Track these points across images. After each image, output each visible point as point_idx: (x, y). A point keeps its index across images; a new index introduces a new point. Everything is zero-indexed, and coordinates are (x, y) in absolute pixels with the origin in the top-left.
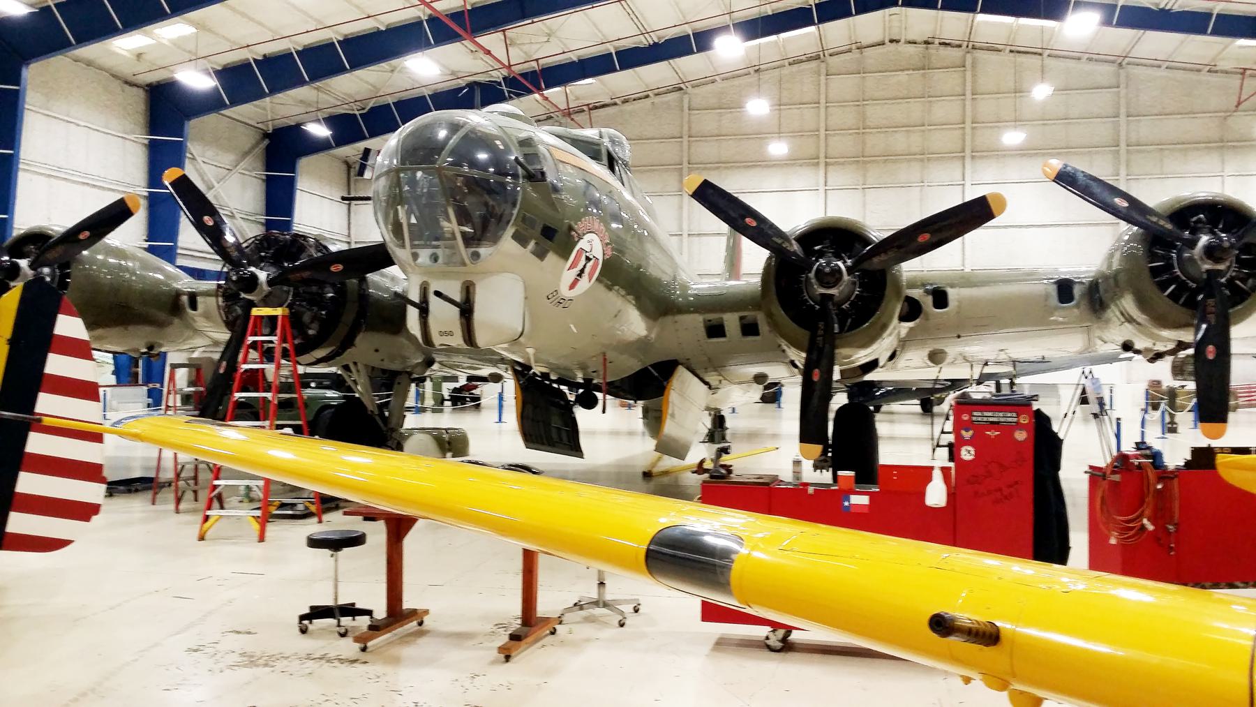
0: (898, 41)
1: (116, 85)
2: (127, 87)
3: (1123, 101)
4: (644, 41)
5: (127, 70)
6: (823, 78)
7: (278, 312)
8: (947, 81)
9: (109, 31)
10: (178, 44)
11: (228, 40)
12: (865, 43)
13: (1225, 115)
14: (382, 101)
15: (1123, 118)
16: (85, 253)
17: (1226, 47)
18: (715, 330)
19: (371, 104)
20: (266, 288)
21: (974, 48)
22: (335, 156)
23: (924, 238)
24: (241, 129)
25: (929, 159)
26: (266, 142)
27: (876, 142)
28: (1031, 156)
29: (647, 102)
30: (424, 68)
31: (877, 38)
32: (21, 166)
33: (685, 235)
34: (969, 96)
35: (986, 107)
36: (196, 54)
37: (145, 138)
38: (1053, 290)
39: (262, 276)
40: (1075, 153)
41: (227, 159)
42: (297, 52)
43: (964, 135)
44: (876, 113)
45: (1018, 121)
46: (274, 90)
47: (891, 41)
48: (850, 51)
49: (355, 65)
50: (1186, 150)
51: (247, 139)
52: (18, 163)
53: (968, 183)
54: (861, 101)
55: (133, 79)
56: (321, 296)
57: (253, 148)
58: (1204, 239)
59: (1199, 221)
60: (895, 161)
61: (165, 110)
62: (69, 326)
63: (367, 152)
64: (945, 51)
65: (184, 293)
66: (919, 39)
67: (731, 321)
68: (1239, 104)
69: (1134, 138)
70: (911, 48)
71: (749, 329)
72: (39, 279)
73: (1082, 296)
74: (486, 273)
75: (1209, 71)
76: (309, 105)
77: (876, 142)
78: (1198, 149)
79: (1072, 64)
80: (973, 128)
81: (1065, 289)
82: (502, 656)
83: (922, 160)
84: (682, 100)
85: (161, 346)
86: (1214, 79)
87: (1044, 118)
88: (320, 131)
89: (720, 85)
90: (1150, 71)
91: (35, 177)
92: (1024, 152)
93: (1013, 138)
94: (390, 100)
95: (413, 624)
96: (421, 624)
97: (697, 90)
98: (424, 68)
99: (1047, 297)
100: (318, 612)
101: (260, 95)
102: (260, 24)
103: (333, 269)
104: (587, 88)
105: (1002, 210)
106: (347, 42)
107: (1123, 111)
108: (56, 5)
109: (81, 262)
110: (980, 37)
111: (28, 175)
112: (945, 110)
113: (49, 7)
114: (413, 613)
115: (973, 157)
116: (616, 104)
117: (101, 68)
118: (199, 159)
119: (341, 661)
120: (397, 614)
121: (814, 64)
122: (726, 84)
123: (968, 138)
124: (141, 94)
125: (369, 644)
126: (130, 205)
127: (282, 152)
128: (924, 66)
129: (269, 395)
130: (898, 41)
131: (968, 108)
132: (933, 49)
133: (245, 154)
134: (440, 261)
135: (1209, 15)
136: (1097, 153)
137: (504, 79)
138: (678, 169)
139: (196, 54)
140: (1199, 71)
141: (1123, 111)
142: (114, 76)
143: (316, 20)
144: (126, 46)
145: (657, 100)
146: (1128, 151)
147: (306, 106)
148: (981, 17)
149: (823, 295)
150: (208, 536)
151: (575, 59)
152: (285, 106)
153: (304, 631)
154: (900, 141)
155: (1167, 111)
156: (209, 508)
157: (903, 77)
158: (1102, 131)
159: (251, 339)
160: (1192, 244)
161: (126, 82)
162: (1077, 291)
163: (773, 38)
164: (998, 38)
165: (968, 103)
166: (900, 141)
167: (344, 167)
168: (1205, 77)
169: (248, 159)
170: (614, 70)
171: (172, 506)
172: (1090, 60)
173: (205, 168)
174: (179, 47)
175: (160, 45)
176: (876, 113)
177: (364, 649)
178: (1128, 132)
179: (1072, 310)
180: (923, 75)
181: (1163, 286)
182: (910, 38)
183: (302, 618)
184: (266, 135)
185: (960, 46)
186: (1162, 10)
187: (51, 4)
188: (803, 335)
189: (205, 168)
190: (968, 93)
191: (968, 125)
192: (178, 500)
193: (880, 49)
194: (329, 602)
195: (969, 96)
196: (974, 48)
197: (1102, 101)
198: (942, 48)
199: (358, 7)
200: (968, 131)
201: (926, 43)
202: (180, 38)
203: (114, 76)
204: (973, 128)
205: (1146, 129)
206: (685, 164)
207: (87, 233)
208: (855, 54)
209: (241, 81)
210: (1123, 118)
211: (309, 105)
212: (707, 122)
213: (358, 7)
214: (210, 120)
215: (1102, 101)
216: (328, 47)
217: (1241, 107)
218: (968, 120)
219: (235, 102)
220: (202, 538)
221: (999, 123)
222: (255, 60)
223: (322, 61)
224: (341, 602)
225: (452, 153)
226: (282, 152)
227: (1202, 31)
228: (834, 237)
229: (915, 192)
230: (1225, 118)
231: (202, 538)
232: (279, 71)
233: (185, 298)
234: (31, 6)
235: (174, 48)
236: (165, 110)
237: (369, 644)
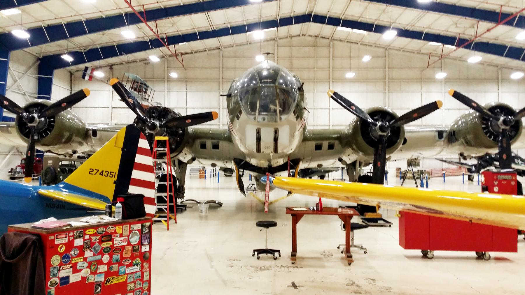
0: (305, 35)
3: (387, 63)
4: (210, 29)
6: (276, 48)
8: (324, 52)
10: (10, 18)
11: (34, 17)
12: (293, 35)
13: (423, 69)
14: (95, 47)
17: (425, 45)
18: (318, 147)
19: (90, 48)
20: (159, 129)
22: (67, 70)
23: (415, 115)
24: (29, 56)
26: (39, 62)
27: (395, 73)
29: (205, 53)
30: (128, 34)
31: (298, 33)
33: (221, 108)
35: (338, 62)
38: (437, 134)
39: (157, 123)
41: (22, 69)
45: (350, 69)
46: (52, 40)
47: (303, 35)
49: (91, 31)
51: (31, 60)
54: (291, 58)
56: (177, 132)
57: (34, 64)
58: (502, 118)
59: (498, 112)
62: (143, 143)
63: (86, 68)
64: (324, 40)
65: (90, 130)
66: (313, 34)
67: (325, 144)
69: (391, 77)
70: (310, 38)
71: (331, 147)
72: (40, 122)
73: (446, 137)
74: (282, 125)
76: (62, 47)
81: (440, 134)
84: (220, 53)
87: (367, 68)
88: (68, 58)
89: (235, 48)
90: (397, 52)
93: (350, 75)
94: (98, 47)
97: (226, 50)
98: (128, 34)
99: (435, 137)
101: (46, 41)
102: (51, 12)
103: (187, 121)
104: (183, 46)
105: (89, 93)
106: (88, 22)
110: (336, 36)
112: (323, 63)
115: (168, 81)
116: (192, 53)
121: (273, 42)
122: (238, 47)
123: (331, 74)
127: (47, 66)
130: (305, 35)
133: (30, 68)
134: (266, 120)
137: (150, 40)
138: (219, 81)
140: (414, 53)
145: (210, 52)
147: (63, 48)
149: (380, 135)
152: (50, 48)
157: (307, 49)
160: (498, 119)
162: (445, 135)
164: (343, 37)
167: (69, 74)
168: (416, 55)
169: (32, 69)
170: (197, 39)
172: (376, 46)
176: (297, 63)
179: (442, 142)
181: (486, 133)
182: (311, 34)
184: (39, 59)
188: (372, 150)
193: (298, 38)
197: (380, 62)
201: (316, 36)
205: (395, 73)
206: (221, 79)
208: (289, 39)
209: (40, 34)
211: (62, 47)
212: (230, 62)
215: (380, 62)
216: (80, 23)
221: (344, 69)
223: (76, 28)
226: (47, 66)
228: (380, 114)
230: (423, 71)
232: (56, 32)
233: (91, 132)
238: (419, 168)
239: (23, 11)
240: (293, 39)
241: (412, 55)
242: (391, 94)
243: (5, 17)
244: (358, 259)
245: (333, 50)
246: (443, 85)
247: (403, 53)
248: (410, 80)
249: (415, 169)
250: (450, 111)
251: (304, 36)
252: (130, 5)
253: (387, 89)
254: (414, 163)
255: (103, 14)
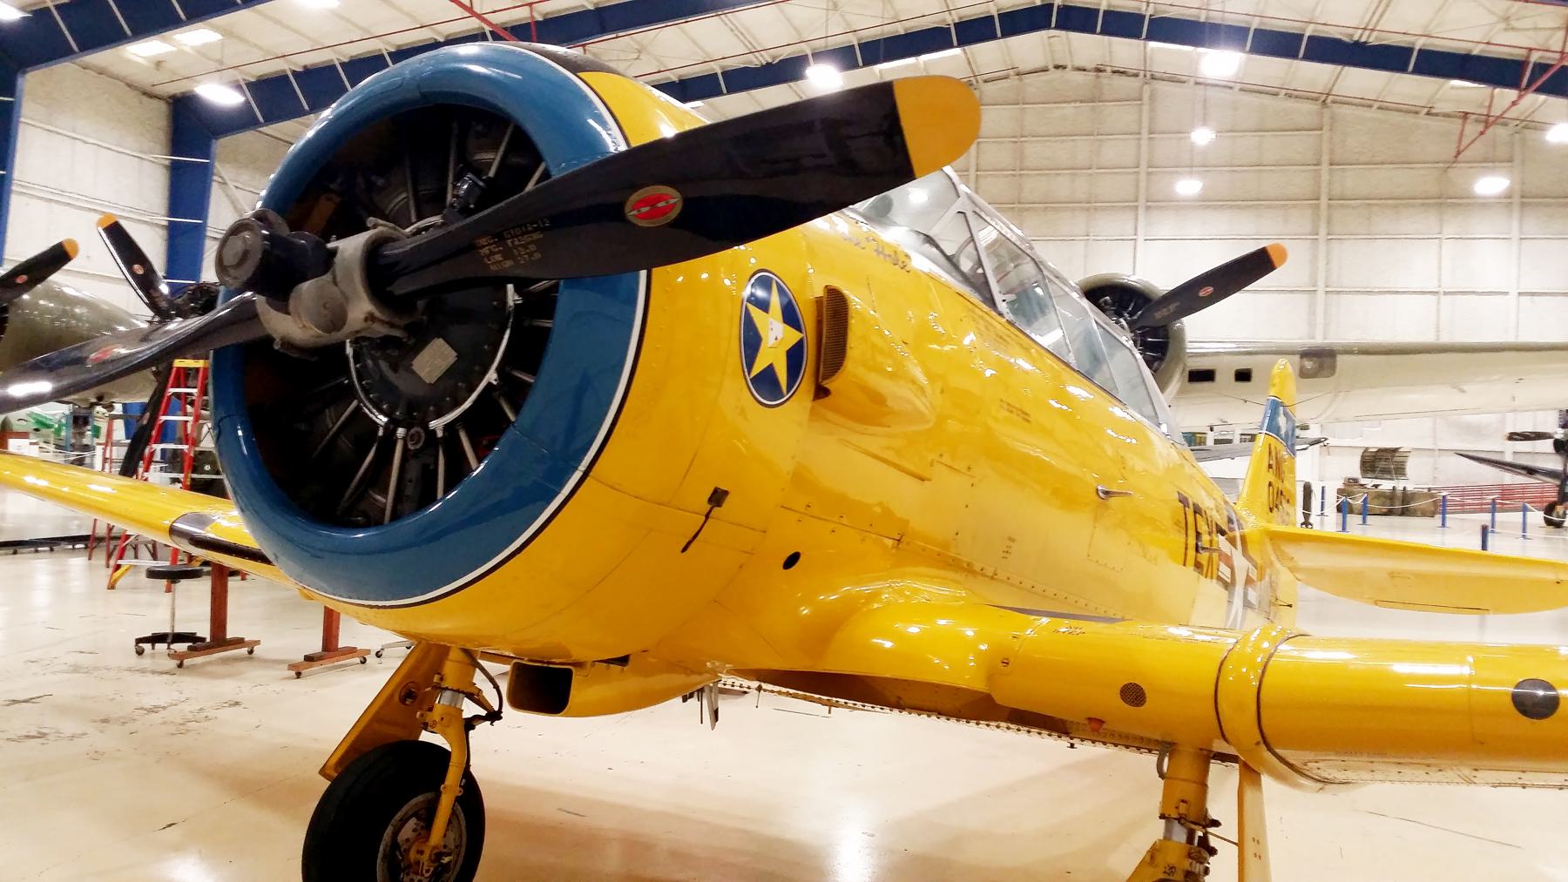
0: (1064, 67)
1: (133, 98)
2: (145, 99)
4: (756, 61)
5: (147, 79)
7: (200, 364)
8: (1119, 116)
9: (115, 37)
10: (202, 51)
11: (261, 49)
12: (1023, 67)
15: (1325, 168)
16: (26, 297)
21: (1153, 78)
25: (1096, 209)
27: (1035, 187)
28: (1216, 208)
31: (1039, 63)
32: (14, 188)
34: (1145, 135)
36: (221, 62)
37: (166, 159)
40: (1269, 207)
42: (342, 64)
43: (1138, 181)
44: (1036, 152)
47: (1057, 67)
48: (1045, 70)
50: (1396, 206)
52: (10, 184)
53: (1140, 239)
54: (1018, 138)
55: (149, 89)
60: (1056, 210)
61: (189, 130)
68: (1459, 153)
69: (1337, 191)
70: (1079, 76)
75: (1428, 114)
77: (1035, 187)
78: (1413, 206)
79: (1267, 100)
80: (1149, 174)
82: (293, 673)
83: (1088, 209)
85: (112, 396)
86: (1430, 121)
90: (1360, 111)
91: (34, 202)
92: (1206, 203)
95: (244, 651)
96: (251, 652)
100: (156, 639)
107: (1325, 158)
108: (57, 7)
109: (22, 306)
110: (1159, 67)
111: (25, 199)
112: (1116, 150)
113: (48, 9)
114: (239, 642)
115: (1148, 208)
117: (117, 78)
118: (231, 184)
119: (153, 672)
120: (219, 640)
123: (1143, 185)
124: (162, 108)
125: (187, 662)
126: (68, 248)
128: (1094, 98)
129: (185, 447)
130: (1064, 67)
131: (1144, 149)
132: (1105, 78)
135: (1409, 50)
136: (1294, 206)
139: (221, 62)
141: (1325, 158)
142: (129, 85)
143: (361, 28)
144: (142, 54)
146: (1330, 206)
148: (1152, 44)
150: (118, 585)
151: (675, 79)
153: (140, 652)
154: (1062, 186)
155: (1377, 159)
156: (121, 557)
157: (1069, 109)
158: (1299, 181)
159: (172, 390)
161: (145, 93)
163: (911, 60)
165: (1144, 143)
166: (1062, 186)
170: (720, 93)
171: (103, 562)
173: (239, 194)
174: (204, 55)
175: (181, 53)
176: (1036, 152)
177: (180, 666)
178: (1330, 183)
180: (1093, 108)
182: (1079, 63)
183: (139, 641)
185: (1136, 75)
186: (1357, 43)
187: (50, 4)
189: (239, 194)
190: (1145, 132)
191: (1143, 168)
192: (109, 556)
193: (1043, 77)
194: (167, 630)
195: (1145, 135)
196: (1153, 78)
198: (1116, 76)
199: (408, 14)
200: (1143, 176)
201: (1098, 70)
202: (205, 45)
203: (129, 85)
204: (1149, 174)
205: (1352, 180)
207: (25, 277)
208: (1014, 81)
210: (1325, 168)
213: (408, 14)
214: (247, 137)
215: (1300, 145)
217: (1461, 157)
218: (1144, 164)
219: (271, 118)
220: (112, 587)
222: (294, 73)
224: (178, 630)
225: (295, 225)
227: (1402, 68)
229: (1079, 247)
231: (112, 587)
234: (22, 9)
235: (200, 58)
236: (189, 130)
237: (187, 662)
238: (1400, 485)
239: (227, 33)
240: (1029, 79)
241: (1410, 119)
242: (1335, 244)
243: (187, 49)
244: (61, 573)
245: (1152, 110)
246: (1516, 215)
247: (1380, 115)
248: (1401, 202)
249: (1386, 485)
250: (1536, 298)
251: (1059, 71)
252: (470, 9)
253: (1323, 231)
254: (1382, 464)
255: (439, 33)
